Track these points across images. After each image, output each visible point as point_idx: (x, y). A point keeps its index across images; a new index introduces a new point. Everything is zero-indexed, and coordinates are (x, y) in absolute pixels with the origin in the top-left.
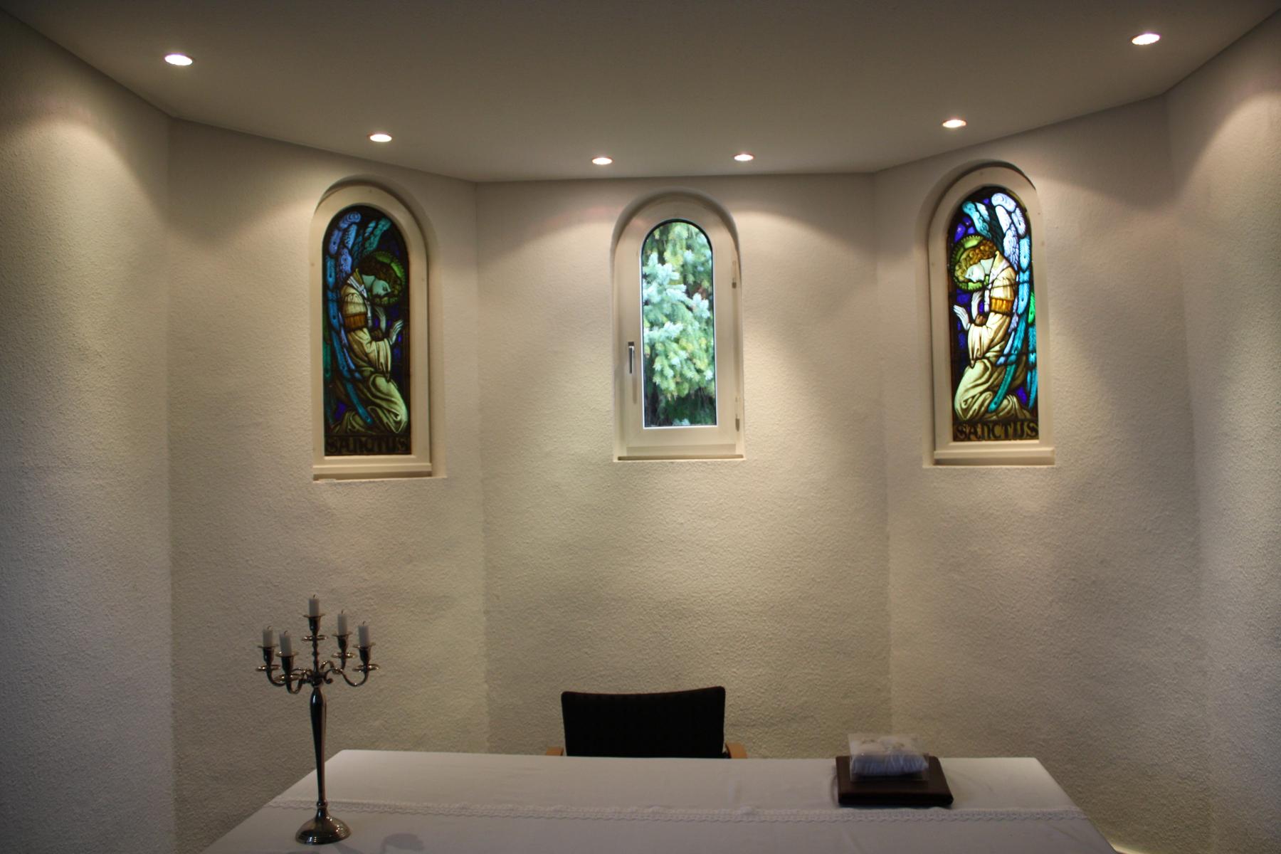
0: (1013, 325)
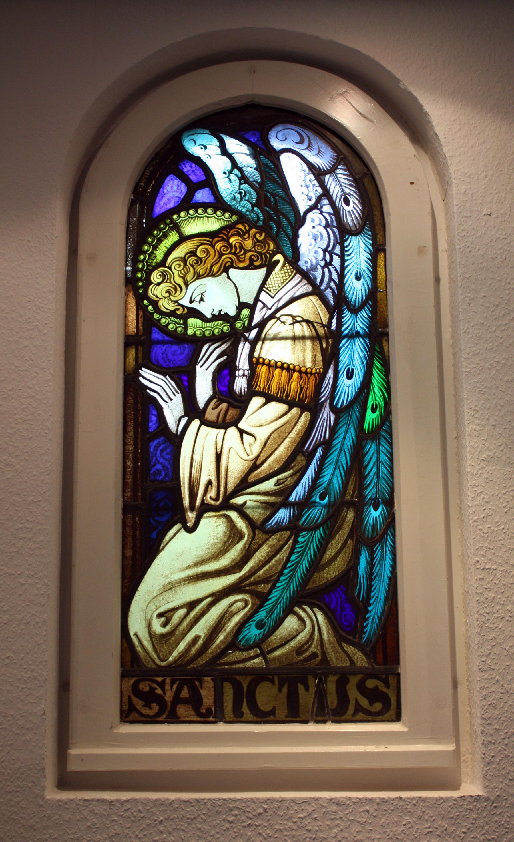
0: (322, 430)
